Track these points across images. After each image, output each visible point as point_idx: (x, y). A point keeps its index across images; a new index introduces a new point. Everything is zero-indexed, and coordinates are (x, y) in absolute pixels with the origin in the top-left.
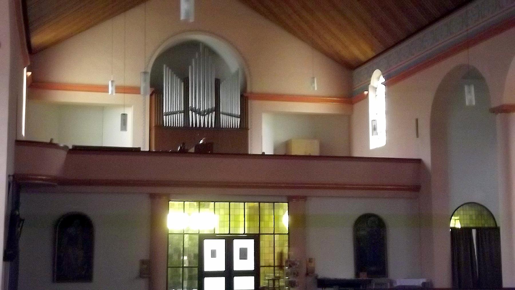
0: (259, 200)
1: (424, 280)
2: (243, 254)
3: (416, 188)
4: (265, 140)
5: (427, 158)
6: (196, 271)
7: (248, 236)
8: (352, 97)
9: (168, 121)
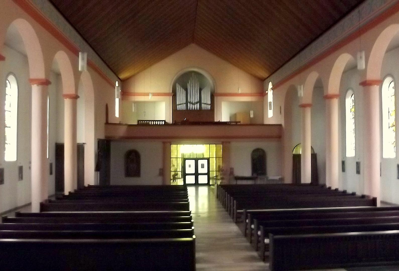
0: (170, 158)
2: (203, 166)
4: (224, 114)
5: (283, 124)
9: (179, 107)
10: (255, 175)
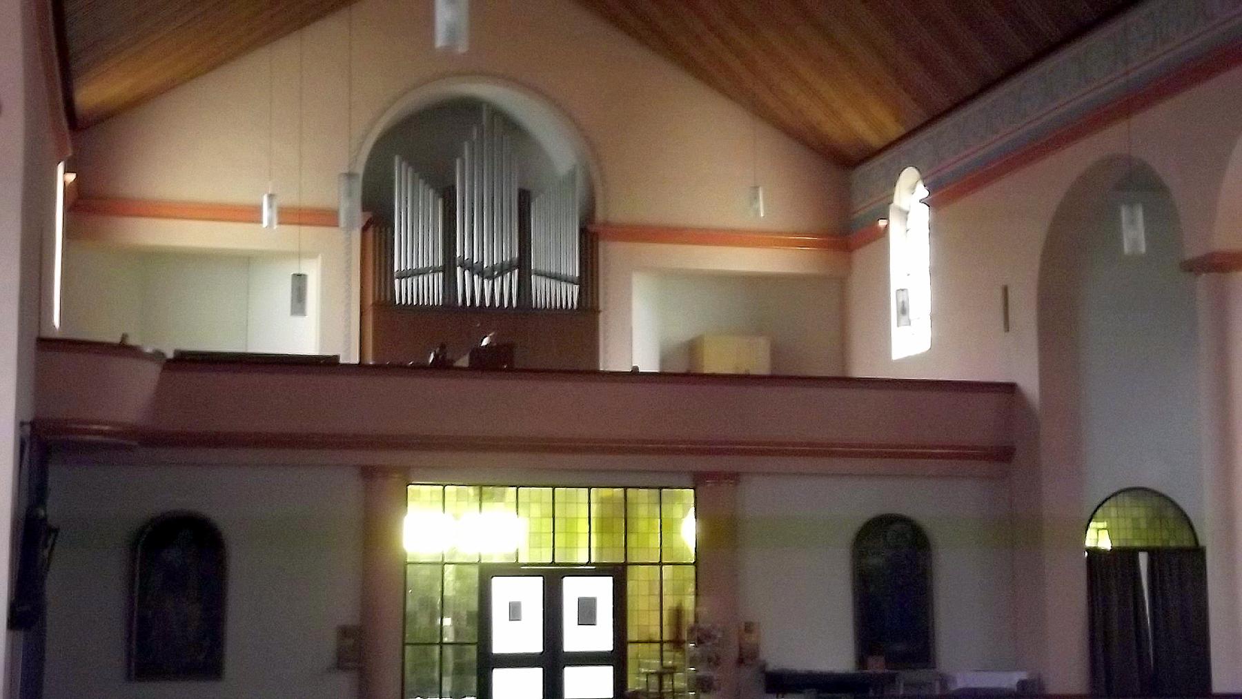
1: (1023, 676)
2: (587, 613)
3: (1003, 454)
4: (638, 338)
5: (1029, 382)
6: (472, 654)
7: (599, 570)
8: (849, 233)
9: (404, 291)
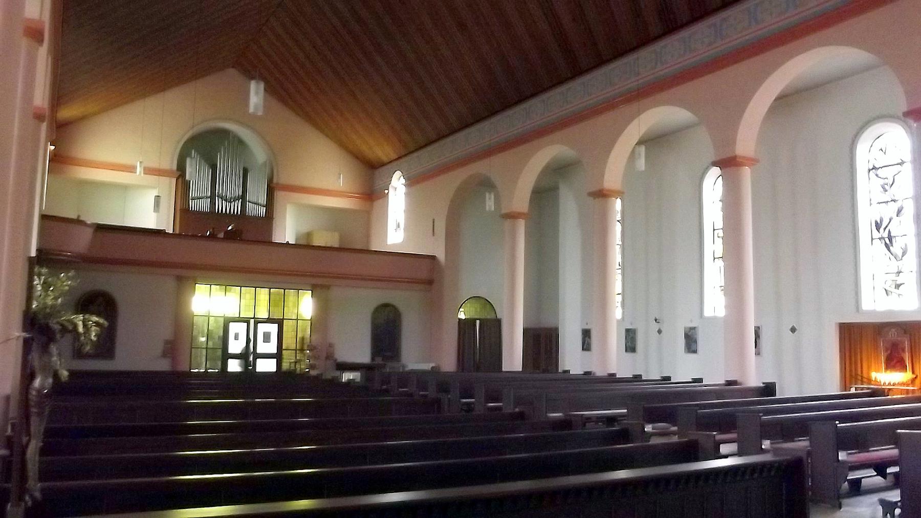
1: (433, 365)
3: (430, 282)
4: (287, 230)
5: (441, 255)
6: (219, 353)
7: (269, 320)
8: (372, 195)
9: (194, 205)
10: (379, 361)
